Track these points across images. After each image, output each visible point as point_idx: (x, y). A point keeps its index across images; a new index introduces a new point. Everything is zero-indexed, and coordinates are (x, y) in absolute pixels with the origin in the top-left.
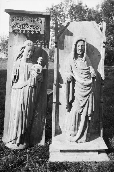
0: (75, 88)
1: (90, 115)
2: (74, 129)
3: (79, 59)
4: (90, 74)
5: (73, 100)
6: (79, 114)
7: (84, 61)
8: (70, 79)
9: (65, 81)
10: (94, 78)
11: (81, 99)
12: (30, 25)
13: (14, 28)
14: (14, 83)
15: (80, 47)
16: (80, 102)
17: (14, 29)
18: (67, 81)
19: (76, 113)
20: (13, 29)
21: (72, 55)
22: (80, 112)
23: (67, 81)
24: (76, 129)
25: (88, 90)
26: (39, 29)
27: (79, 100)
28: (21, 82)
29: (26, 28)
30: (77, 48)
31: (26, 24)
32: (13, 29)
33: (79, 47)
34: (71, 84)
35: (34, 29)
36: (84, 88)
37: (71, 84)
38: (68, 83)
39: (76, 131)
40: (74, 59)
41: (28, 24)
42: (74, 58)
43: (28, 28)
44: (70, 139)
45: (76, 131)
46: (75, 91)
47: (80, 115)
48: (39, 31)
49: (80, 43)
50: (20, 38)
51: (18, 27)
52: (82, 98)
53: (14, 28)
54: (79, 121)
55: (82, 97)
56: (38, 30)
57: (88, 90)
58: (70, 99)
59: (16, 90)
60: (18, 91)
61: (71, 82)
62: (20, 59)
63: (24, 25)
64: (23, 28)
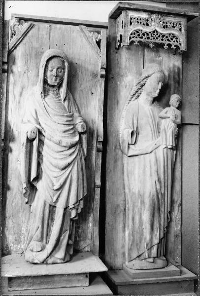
0: (44, 153)
1: (73, 206)
2: (40, 236)
3: (51, 98)
4: (74, 125)
5: (38, 178)
6: (50, 205)
7: (63, 100)
8: (34, 133)
9: (24, 140)
10: (80, 134)
11: (56, 175)
12: (161, 34)
13: (133, 37)
14: (131, 146)
15: (55, 70)
16: (54, 180)
17: (132, 39)
18: (27, 137)
19: (45, 204)
20: (131, 40)
21: (39, 88)
22: (54, 201)
23: (27, 137)
24: (44, 237)
25: (71, 155)
26: (177, 41)
27: (51, 178)
28: (145, 143)
29: (154, 38)
30: (49, 73)
31: (154, 32)
32: (131, 40)
33: (52, 71)
34: (35, 143)
35: (168, 40)
36: (62, 151)
37: (35, 143)
38: (30, 141)
39: (45, 240)
40: (43, 94)
41: (157, 32)
42: (42, 93)
43: (157, 38)
44: (32, 258)
45: (45, 240)
46: (44, 159)
47: (52, 208)
48: (178, 44)
49: (54, 64)
50: (72, 58)
51: (139, 35)
52: (57, 173)
53: (133, 37)
54: (51, 218)
55: (58, 170)
56: (176, 43)
57: (71, 155)
58: (33, 175)
59: (140, 158)
60: (144, 158)
61: (34, 139)
62: (136, 100)
63: (150, 33)
64: (148, 38)
